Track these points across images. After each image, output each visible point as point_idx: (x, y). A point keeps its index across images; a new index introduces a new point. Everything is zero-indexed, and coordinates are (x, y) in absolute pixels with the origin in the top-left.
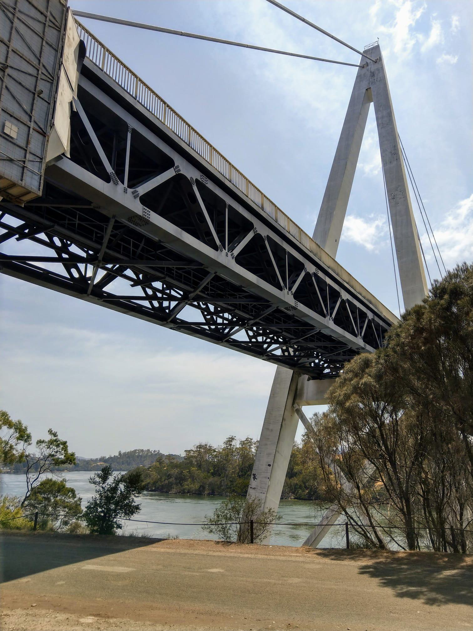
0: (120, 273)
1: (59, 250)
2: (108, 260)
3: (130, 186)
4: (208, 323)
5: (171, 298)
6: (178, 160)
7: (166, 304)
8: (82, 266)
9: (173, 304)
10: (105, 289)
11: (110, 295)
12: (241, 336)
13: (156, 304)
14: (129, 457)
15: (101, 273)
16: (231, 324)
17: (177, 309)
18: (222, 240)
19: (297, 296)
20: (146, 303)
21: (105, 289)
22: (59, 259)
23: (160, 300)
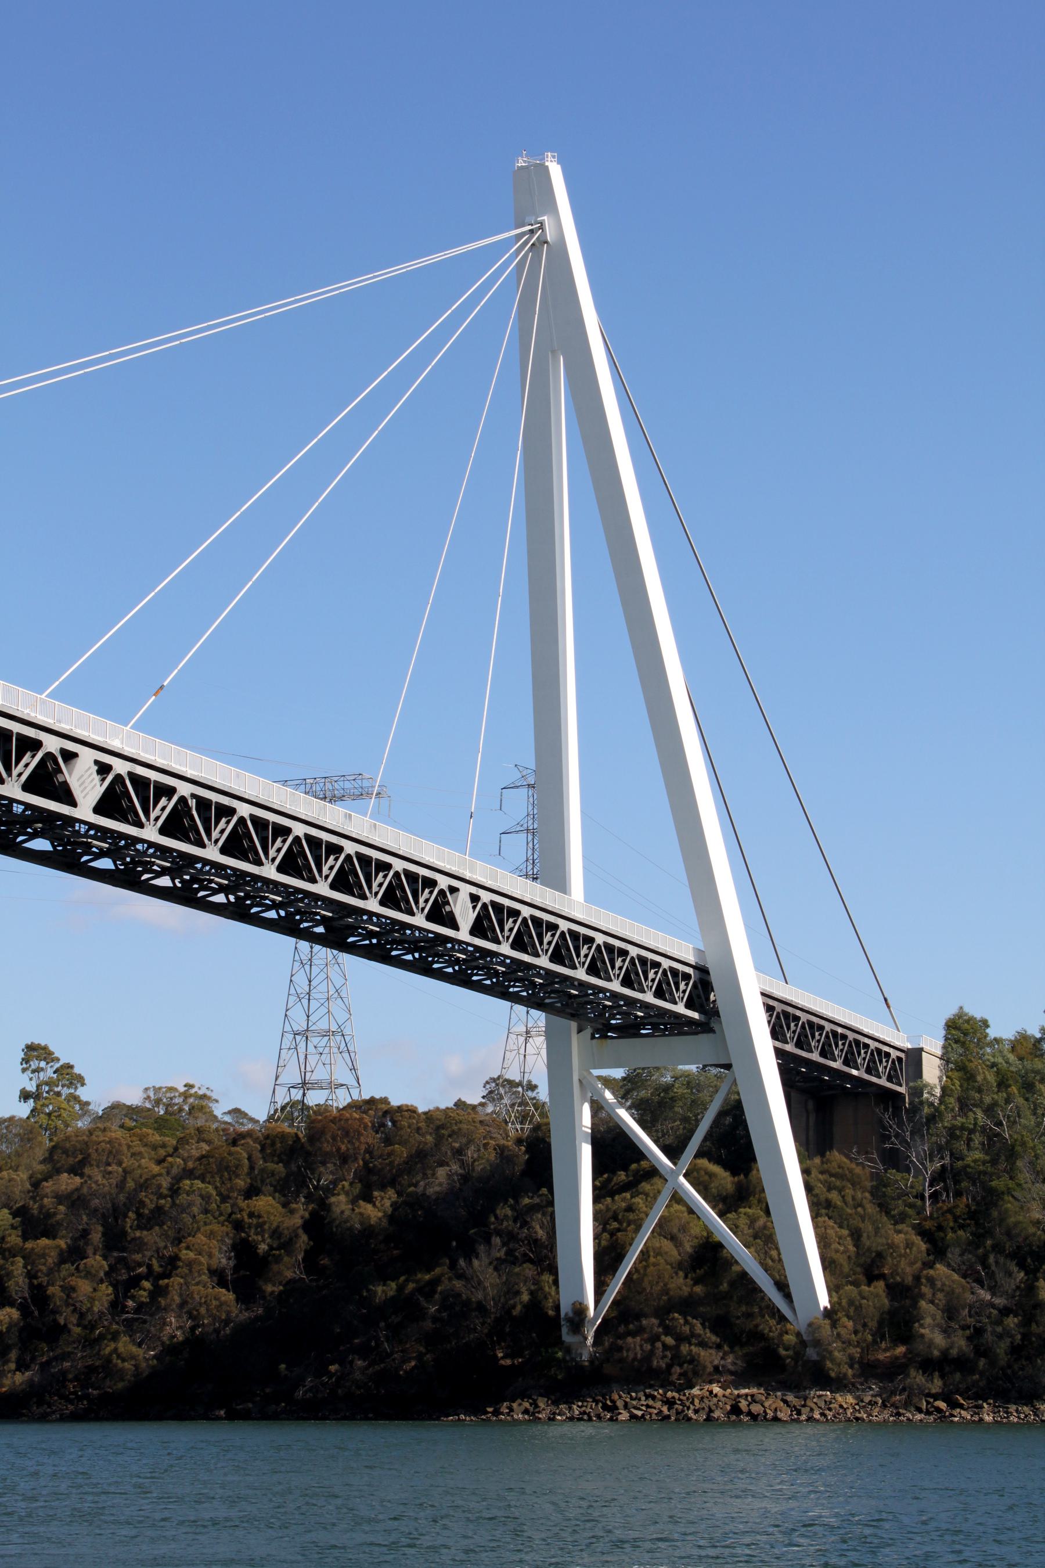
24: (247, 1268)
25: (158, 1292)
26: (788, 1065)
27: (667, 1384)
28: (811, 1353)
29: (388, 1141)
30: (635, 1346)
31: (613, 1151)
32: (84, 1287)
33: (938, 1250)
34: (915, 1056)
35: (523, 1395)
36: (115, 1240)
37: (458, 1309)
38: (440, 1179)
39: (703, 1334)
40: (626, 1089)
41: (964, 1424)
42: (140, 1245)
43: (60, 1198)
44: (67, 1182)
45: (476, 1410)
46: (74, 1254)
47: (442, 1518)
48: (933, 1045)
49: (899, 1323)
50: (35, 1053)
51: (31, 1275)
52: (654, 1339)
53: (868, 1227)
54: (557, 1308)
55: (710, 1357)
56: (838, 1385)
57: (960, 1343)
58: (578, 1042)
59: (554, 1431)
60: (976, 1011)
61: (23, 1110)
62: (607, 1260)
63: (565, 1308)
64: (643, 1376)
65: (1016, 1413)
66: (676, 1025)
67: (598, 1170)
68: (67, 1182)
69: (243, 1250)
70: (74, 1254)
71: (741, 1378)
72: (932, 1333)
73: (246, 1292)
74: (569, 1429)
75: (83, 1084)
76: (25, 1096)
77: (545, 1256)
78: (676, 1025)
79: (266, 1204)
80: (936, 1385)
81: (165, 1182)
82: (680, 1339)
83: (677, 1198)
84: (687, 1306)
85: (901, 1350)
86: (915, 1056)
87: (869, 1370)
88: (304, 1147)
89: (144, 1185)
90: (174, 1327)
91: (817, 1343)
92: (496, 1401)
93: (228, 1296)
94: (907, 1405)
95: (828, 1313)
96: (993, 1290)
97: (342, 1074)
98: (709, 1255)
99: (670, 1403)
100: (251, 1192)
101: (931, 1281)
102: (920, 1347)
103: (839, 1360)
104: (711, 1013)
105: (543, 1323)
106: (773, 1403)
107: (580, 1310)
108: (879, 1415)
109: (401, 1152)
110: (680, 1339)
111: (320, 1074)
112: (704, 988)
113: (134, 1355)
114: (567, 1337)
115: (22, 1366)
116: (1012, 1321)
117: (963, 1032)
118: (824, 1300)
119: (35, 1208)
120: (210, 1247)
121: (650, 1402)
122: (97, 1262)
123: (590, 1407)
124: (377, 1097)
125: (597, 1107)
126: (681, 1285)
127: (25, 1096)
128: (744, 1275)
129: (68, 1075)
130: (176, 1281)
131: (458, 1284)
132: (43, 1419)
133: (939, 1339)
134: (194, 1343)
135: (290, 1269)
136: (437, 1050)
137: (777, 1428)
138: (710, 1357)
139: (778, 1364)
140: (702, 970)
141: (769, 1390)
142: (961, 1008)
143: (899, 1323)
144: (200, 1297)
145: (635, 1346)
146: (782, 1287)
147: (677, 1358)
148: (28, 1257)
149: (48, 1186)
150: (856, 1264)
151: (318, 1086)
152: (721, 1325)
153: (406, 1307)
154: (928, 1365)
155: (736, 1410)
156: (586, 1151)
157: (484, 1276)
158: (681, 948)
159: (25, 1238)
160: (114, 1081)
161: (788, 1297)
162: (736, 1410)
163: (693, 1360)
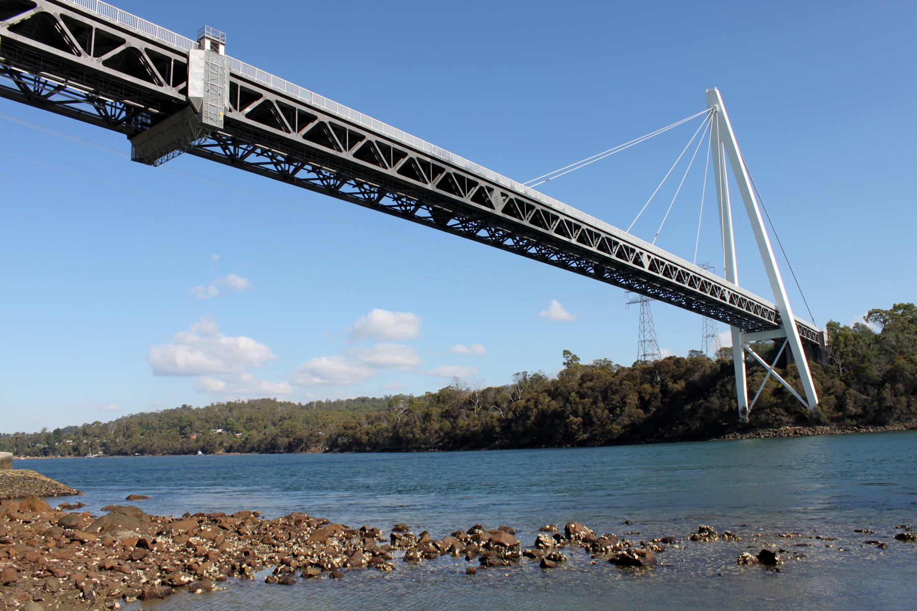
0: (302, 167)
1: (271, 158)
2: (296, 161)
3: (95, 56)
4: (491, 236)
5: (410, 205)
6: (478, 181)
7: (408, 208)
8: (283, 165)
9: (412, 208)
10: (380, 202)
11: (299, 180)
12: (533, 250)
13: (366, 196)
14: (253, 407)
15: (292, 168)
16: (527, 245)
17: (415, 210)
18: (429, 179)
19: (578, 241)
20: (398, 208)
21: (380, 202)
22: (319, 179)
23: (405, 207)
24: (644, 404)
25: (622, 411)
26: (802, 339)
27: (773, 427)
28: (815, 416)
29: (677, 367)
30: (763, 417)
31: (751, 365)
32: (600, 411)
33: (848, 385)
34: (821, 334)
35: (731, 432)
36: (605, 398)
37: (708, 410)
38: (696, 376)
39: (781, 413)
40: (756, 348)
41: (863, 433)
42: (613, 399)
43: (588, 388)
44: (589, 384)
45: (718, 437)
46: (595, 403)
47: (834, 476)
48: (825, 331)
49: (840, 405)
50: (566, 353)
51: (584, 409)
52: (768, 415)
53: (825, 380)
54: (737, 408)
55: (785, 419)
56: (825, 424)
57: (859, 411)
58: (741, 335)
59: (742, 441)
60: (835, 320)
61: (565, 367)
62: (751, 395)
63: (740, 408)
64: (766, 425)
65: (879, 429)
66: (774, 327)
67: (747, 369)
68: (589, 384)
69: (641, 398)
70: (595, 403)
71: (795, 424)
72: (852, 408)
73: (646, 410)
74: (748, 441)
75: (45, 429)
76: (564, 364)
77: (733, 395)
78: (774, 327)
79: (647, 386)
80: (854, 422)
81: (618, 383)
82: (777, 414)
83: (772, 376)
84: (776, 405)
85: (841, 413)
86: (821, 334)
87: (833, 420)
88: (649, 372)
89: (611, 384)
90: (626, 421)
91: (817, 413)
92: (724, 434)
93: (641, 411)
94: (846, 428)
95: (819, 404)
96: (868, 395)
97: (656, 352)
98: (780, 392)
99: (776, 432)
100: (641, 384)
101: (849, 394)
102: (848, 413)
103: (824, 417)
104: (780, 323)
105: (734, 413)
106: (806, 430)
107: (745, 409)
108: (838, 432)
109: (683, 370)
110: (777, 414)
111: (649, 351)
112: (778, 318)
113: (616, 428)
114: (741, 416)
115: (584, 433)
116: (875, 403)
117: (831, 326)
118: (817, 402)
119: (582, 391)
120: (633, 399)
121: (770, 432)
122: (601, 405)
123: (752, 434)
124: (62, 427)
125: (747, 353)
126: (773, 400)
127: (564, 364)
128: (793, 396)
129: (575, 358)
130: (627, 408)
131: (708, 404)
132: (593, 446)
133: (854, 410)
134: (633, 424)
135: (657, 403)
136: (710, 339)
137: (808, 438)
138: (785, 419)
139: (805, 420)
140: (777, 311)
141: (804, 427)
142: (45, 429)
143: (840, 405)
144: (633, 411)
145: (763, 417)
146: (805, 399)
147: (776, 420)
148: (583, 404)
149: (585, 385)
150: (824, 391)
151: (649, 355)
152: (787, 410)
153: (694, 410)
154: (852, 417)
155: (796, 433)
156: (744, 365)
157: (715, 401)
158: (771, 305)
159: (580, 399)
160: (586, 360)
161: (807, 402)
162: (796, 433)
163: (780, 420)
